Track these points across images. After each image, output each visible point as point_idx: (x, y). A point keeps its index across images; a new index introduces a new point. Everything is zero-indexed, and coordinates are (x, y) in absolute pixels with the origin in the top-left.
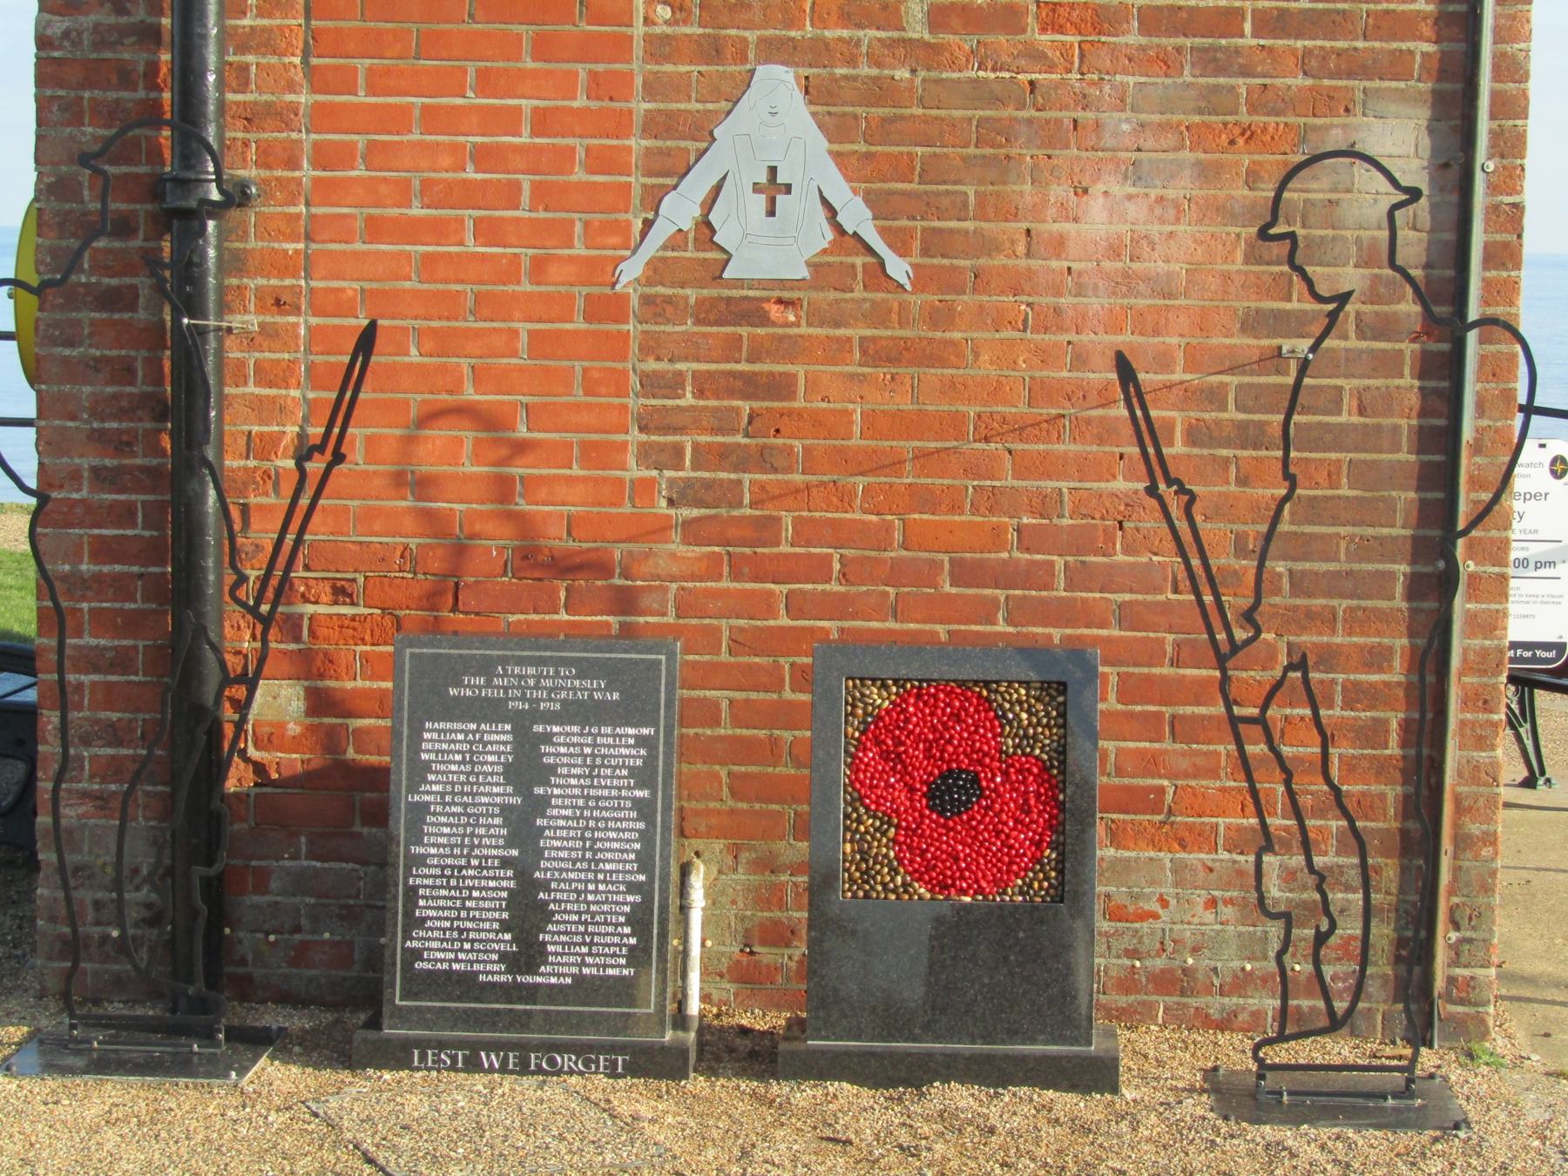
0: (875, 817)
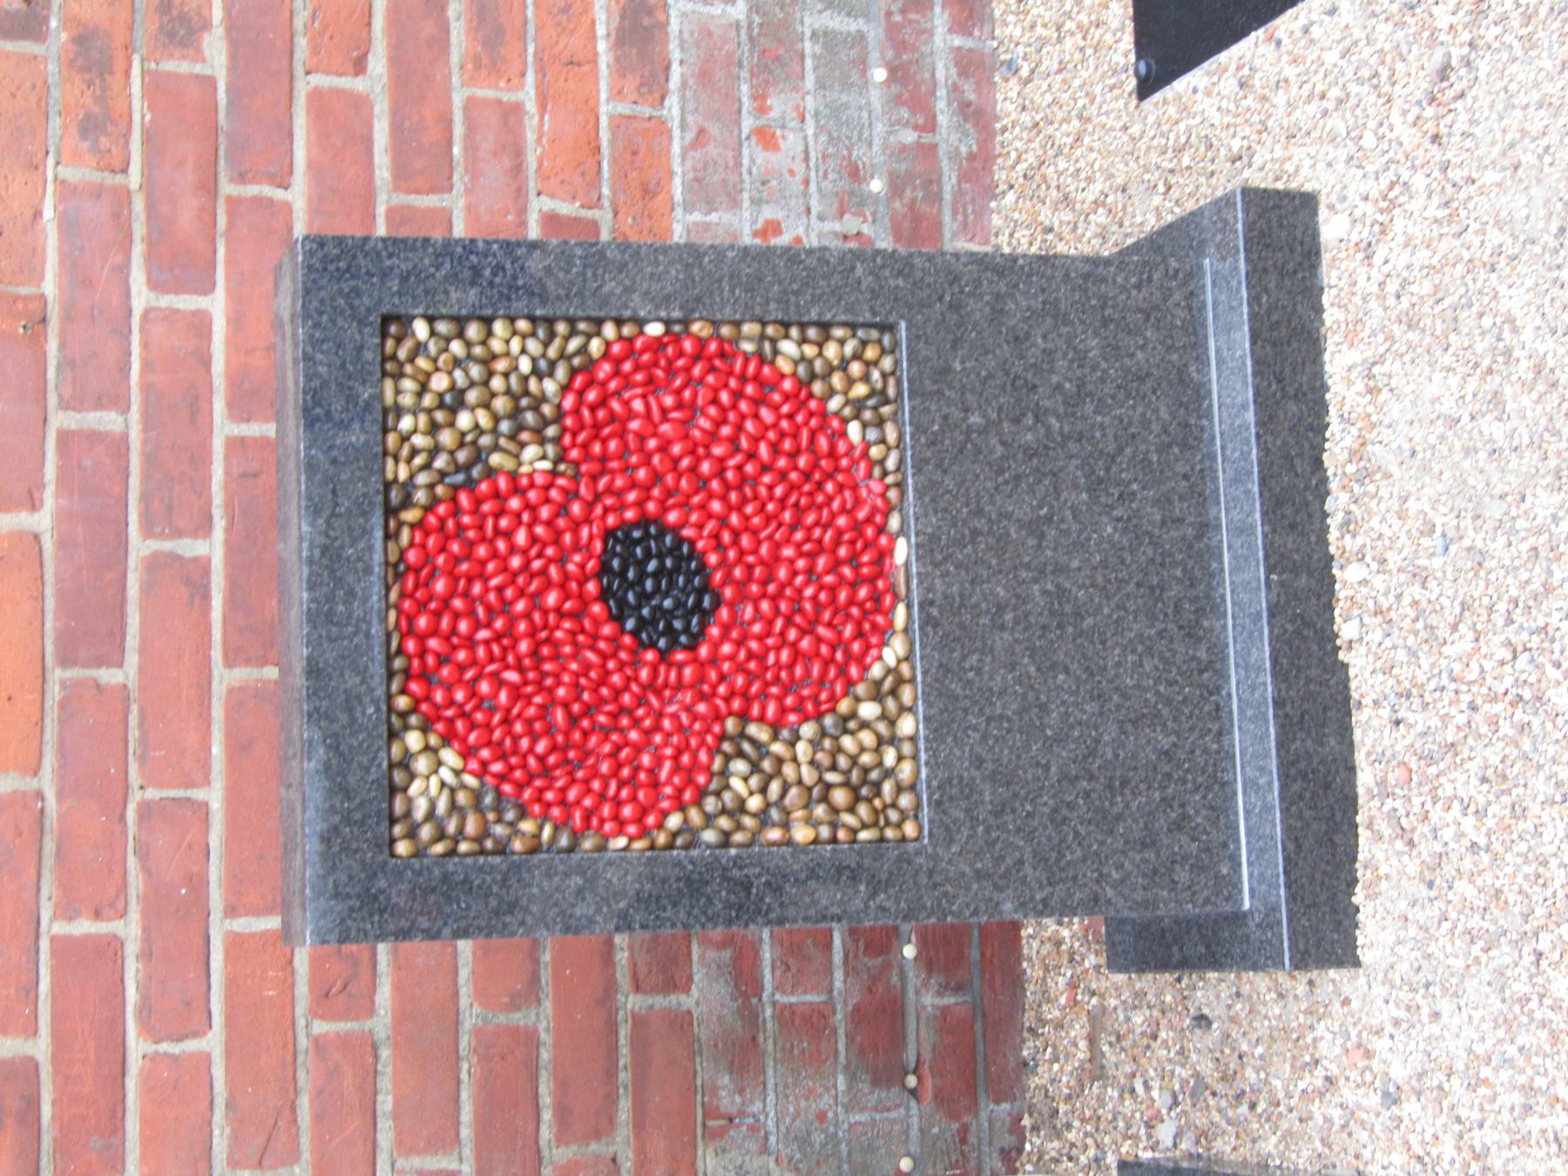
0: (725, 773)
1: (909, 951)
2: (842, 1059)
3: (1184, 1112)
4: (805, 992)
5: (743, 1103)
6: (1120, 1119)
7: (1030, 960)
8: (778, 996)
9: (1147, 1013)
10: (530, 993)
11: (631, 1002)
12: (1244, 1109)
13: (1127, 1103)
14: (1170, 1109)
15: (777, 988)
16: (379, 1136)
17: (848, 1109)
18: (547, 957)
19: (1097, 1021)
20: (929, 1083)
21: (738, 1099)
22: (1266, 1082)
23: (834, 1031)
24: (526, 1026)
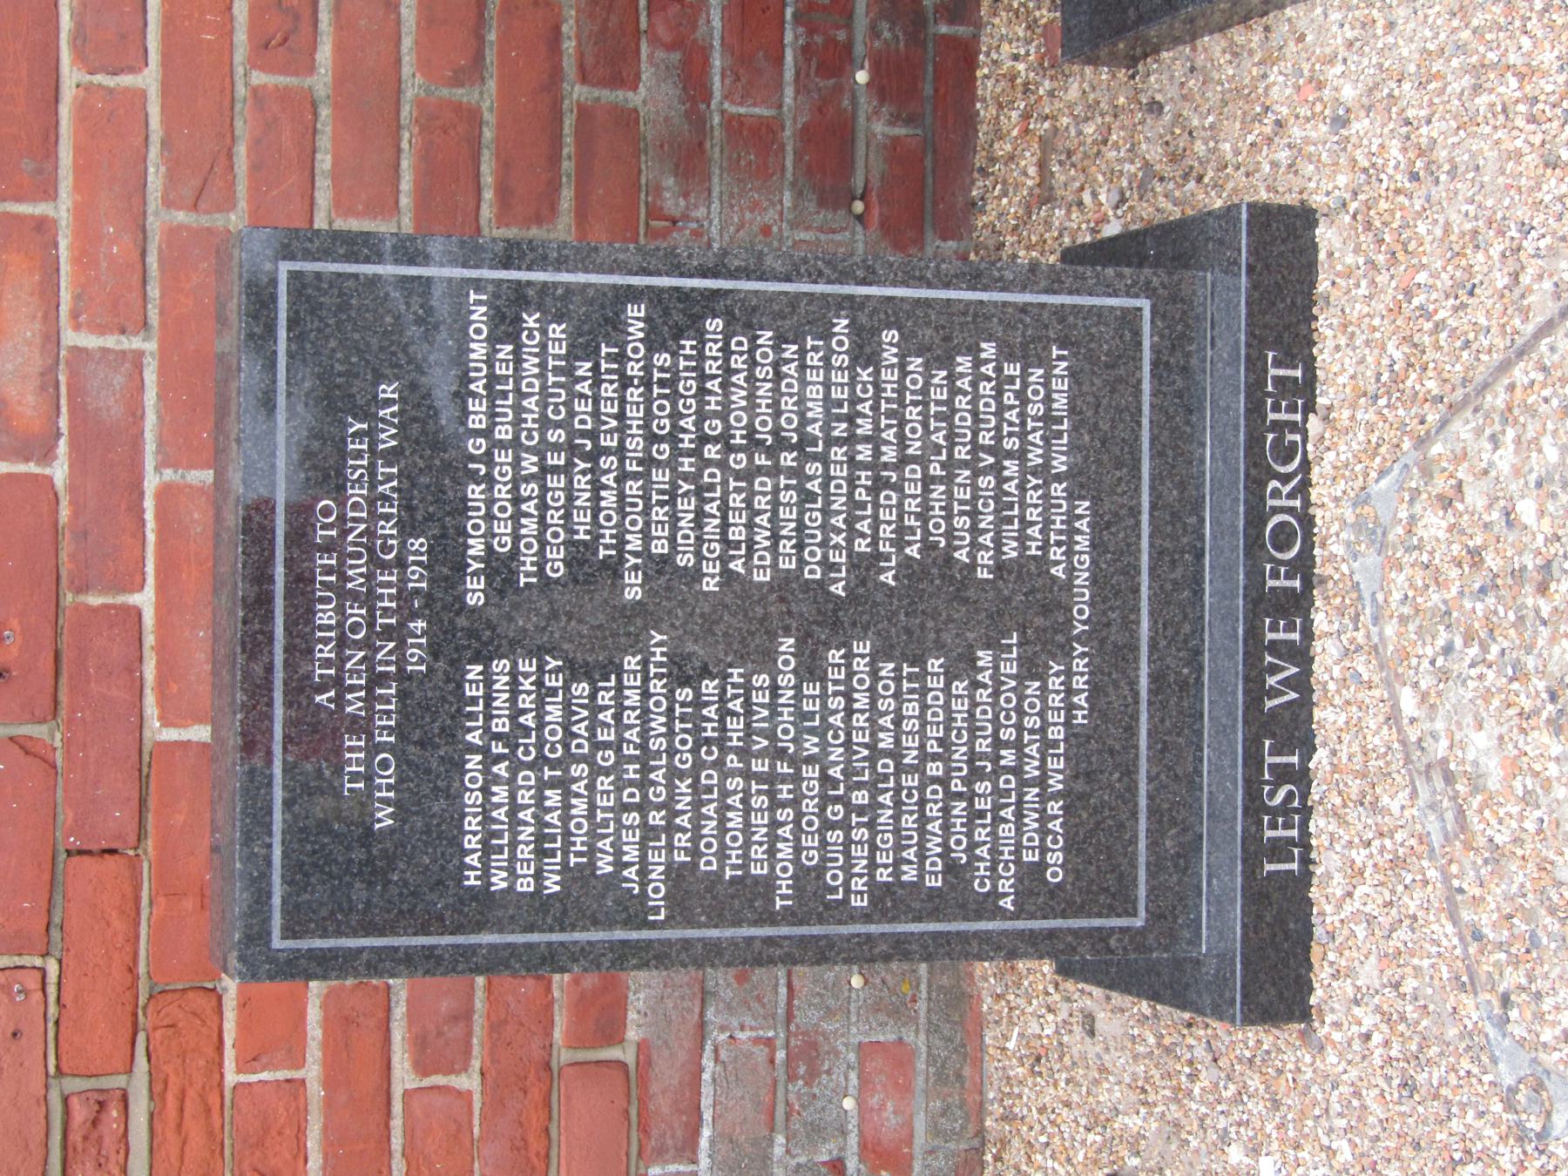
1: (862, 77)
2: (789, 175)
3: (1131, 208)
4: (755, 105)
5: (687, 208)
6: (1066, 233)
7: (984, 100)
8: (726, 105)
9: (1099, 120)
10: (473, 70)
11: (577, 93)
12: (1192, 185)
13: (1074, 216)
14: (1117, 207)
15: (726, 97)
16: (317, 194)
17: (794, 225)
18: (492, 36)
19: (1046, 144)
20: (876, 212)
21: (682, 202)
22: (1215, 149)
23: (782, 148)
24: (469, 103)
